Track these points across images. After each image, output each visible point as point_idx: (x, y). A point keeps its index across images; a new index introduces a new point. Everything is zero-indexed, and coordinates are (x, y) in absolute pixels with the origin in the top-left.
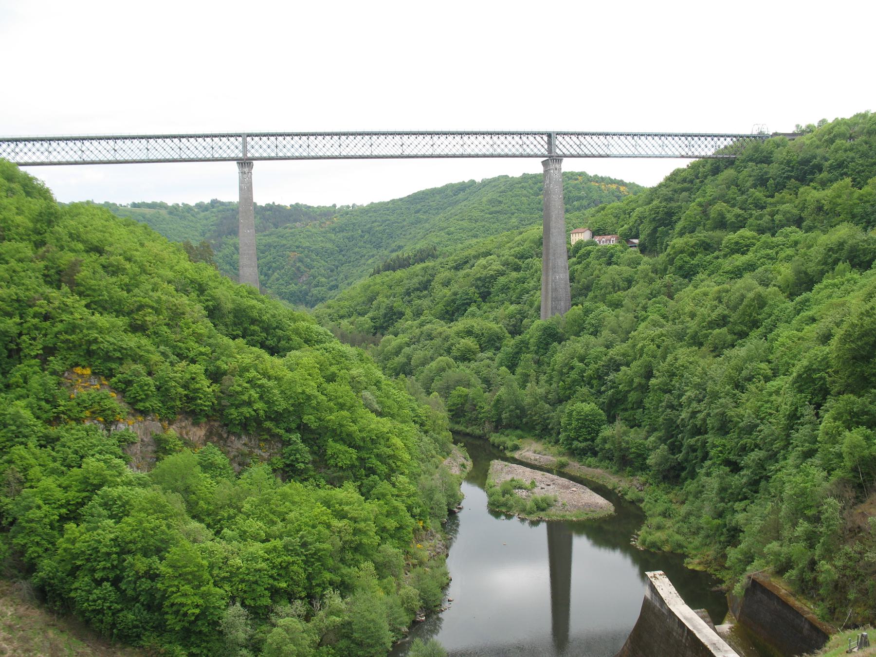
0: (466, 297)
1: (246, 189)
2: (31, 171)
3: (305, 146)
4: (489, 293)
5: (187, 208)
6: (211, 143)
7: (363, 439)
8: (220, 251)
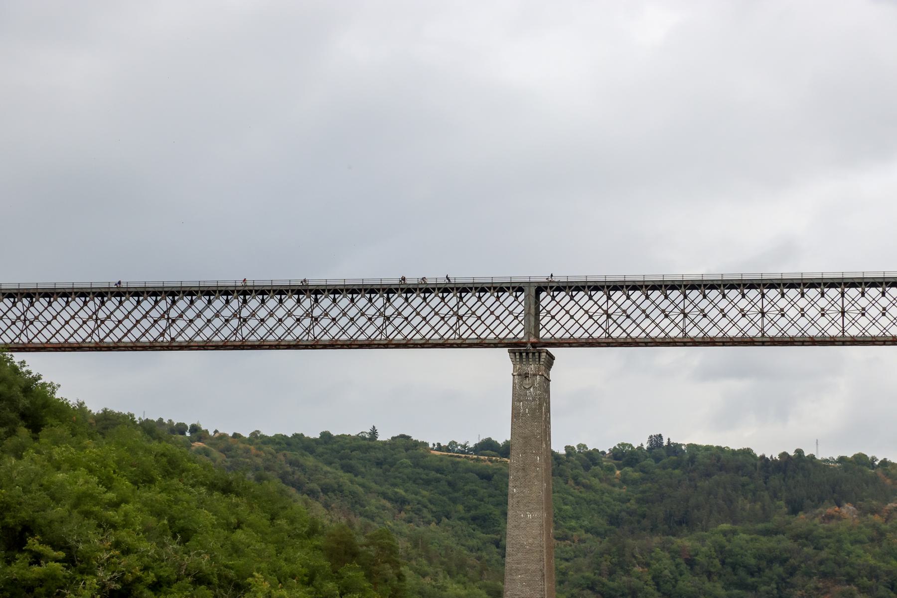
3: (853, 313)
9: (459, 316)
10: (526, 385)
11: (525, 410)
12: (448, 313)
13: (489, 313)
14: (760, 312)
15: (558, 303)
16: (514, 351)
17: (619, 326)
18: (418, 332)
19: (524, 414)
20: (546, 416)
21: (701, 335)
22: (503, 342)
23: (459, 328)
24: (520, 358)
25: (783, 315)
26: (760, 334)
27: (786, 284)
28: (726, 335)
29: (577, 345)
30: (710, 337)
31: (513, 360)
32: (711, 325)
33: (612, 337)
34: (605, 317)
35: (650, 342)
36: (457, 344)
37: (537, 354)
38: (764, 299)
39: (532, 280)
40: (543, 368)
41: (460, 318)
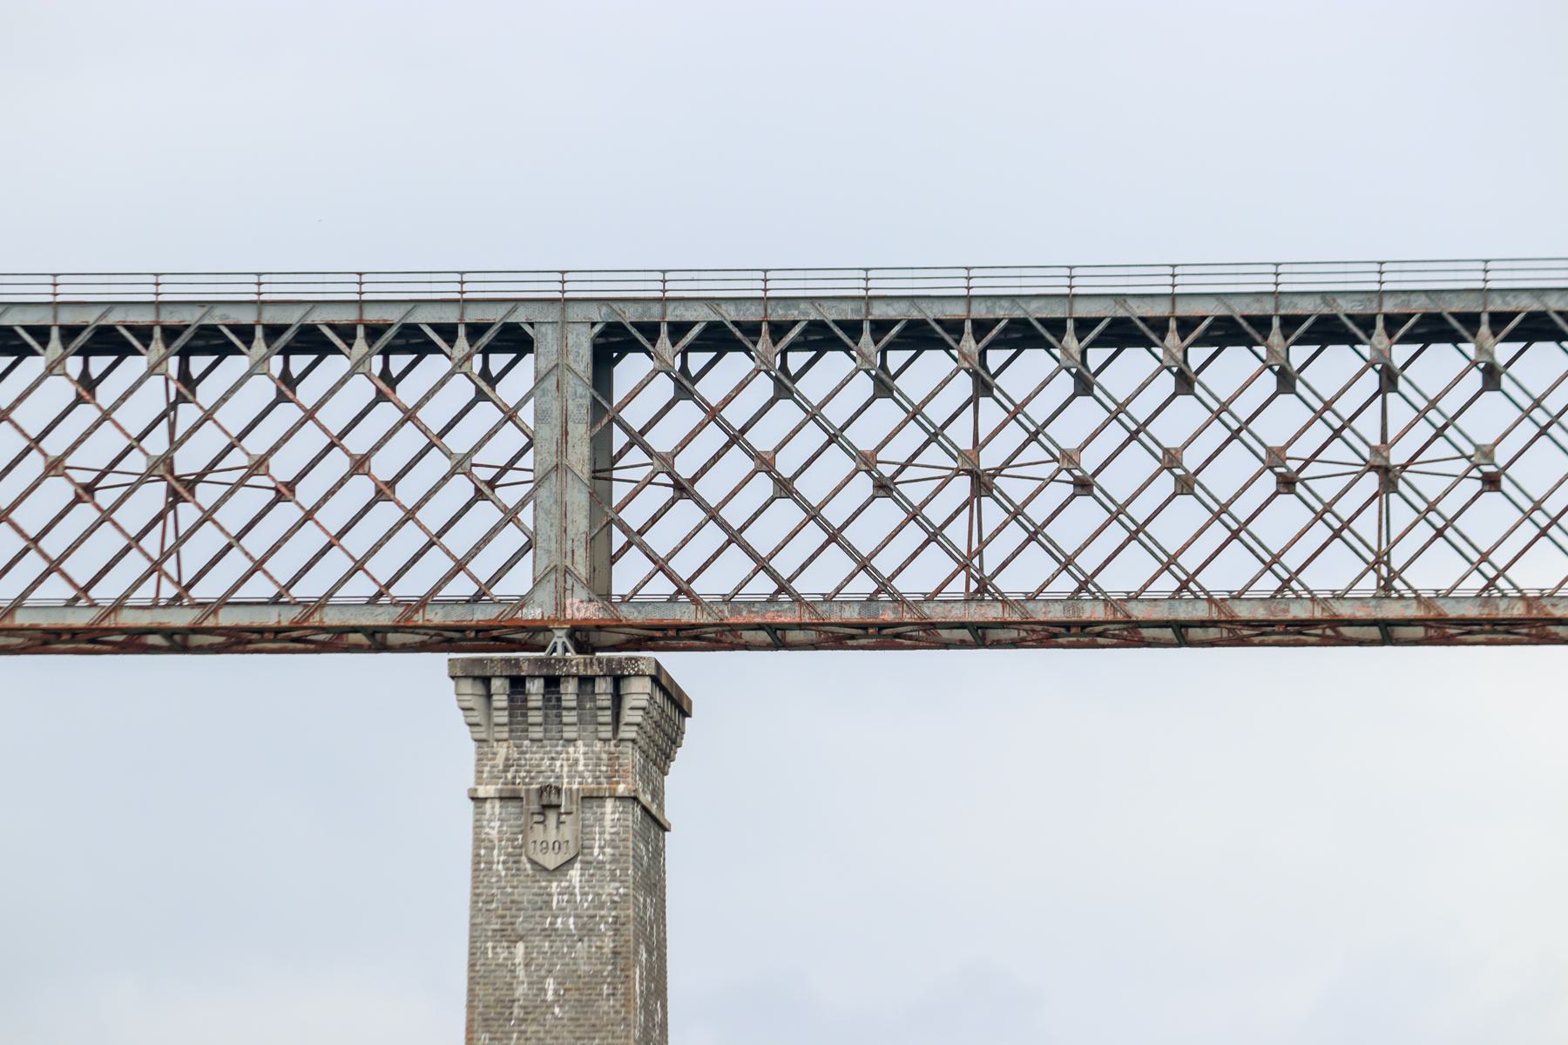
9: (178, 479)
10: (545, 850)
11: (538, 985)
12: (915, 455)
13: (375, 461)
14: (1373, 468)
15: (409, 415)
16: (477, 672)
17: (734, 537)
18: (54, 567)
19: (536, 1009)
20: (649, 1013)
21: (864, 585)
22: (418, 619)
23: (176, 548)
24: (511, 709)
25: (1491, 482)
26: (1370, 583)
27: (1301, 320)
28: (1192, 586)
29: (811, 635)
30: (1523, 598)
31: (477, 717)
32: (1116, 534)
33: (797, 599)
34: (962, 486)
35: (1203, 624)
36: (168, 632)
37: (603, 686)
38: (1391, 397)
39: (575, 289)
40: (631, 758)
41: (181, 490)
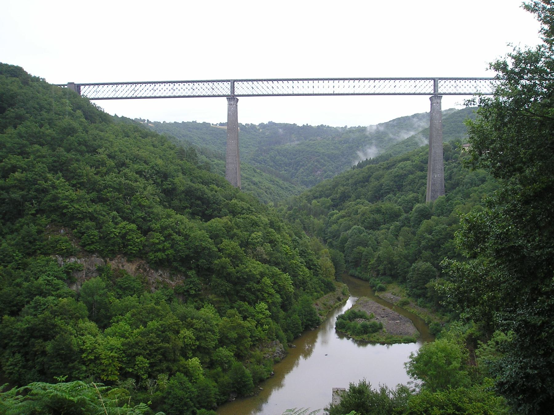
0: (388, 187)
1: (233, 113)
2: (98, 103)
4: (402, 186)
5: (253, 126)
6: (273, 85)
7: (238, 278)
8: (268, 154)
